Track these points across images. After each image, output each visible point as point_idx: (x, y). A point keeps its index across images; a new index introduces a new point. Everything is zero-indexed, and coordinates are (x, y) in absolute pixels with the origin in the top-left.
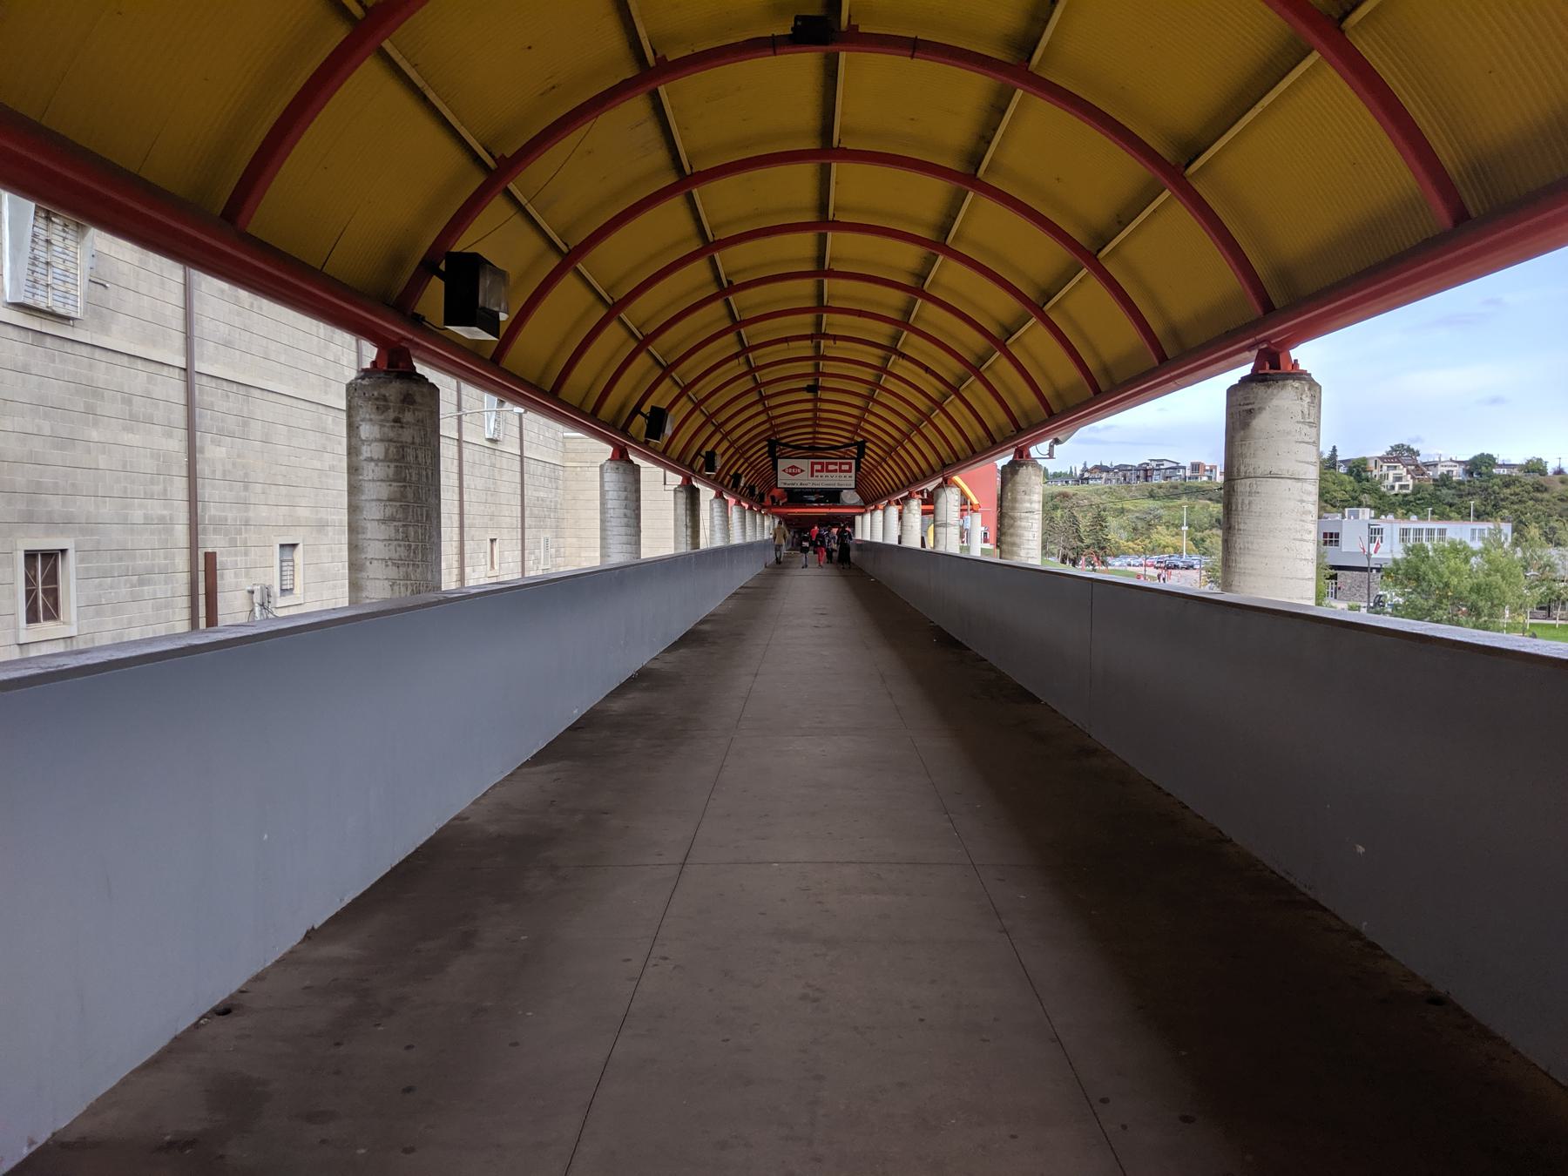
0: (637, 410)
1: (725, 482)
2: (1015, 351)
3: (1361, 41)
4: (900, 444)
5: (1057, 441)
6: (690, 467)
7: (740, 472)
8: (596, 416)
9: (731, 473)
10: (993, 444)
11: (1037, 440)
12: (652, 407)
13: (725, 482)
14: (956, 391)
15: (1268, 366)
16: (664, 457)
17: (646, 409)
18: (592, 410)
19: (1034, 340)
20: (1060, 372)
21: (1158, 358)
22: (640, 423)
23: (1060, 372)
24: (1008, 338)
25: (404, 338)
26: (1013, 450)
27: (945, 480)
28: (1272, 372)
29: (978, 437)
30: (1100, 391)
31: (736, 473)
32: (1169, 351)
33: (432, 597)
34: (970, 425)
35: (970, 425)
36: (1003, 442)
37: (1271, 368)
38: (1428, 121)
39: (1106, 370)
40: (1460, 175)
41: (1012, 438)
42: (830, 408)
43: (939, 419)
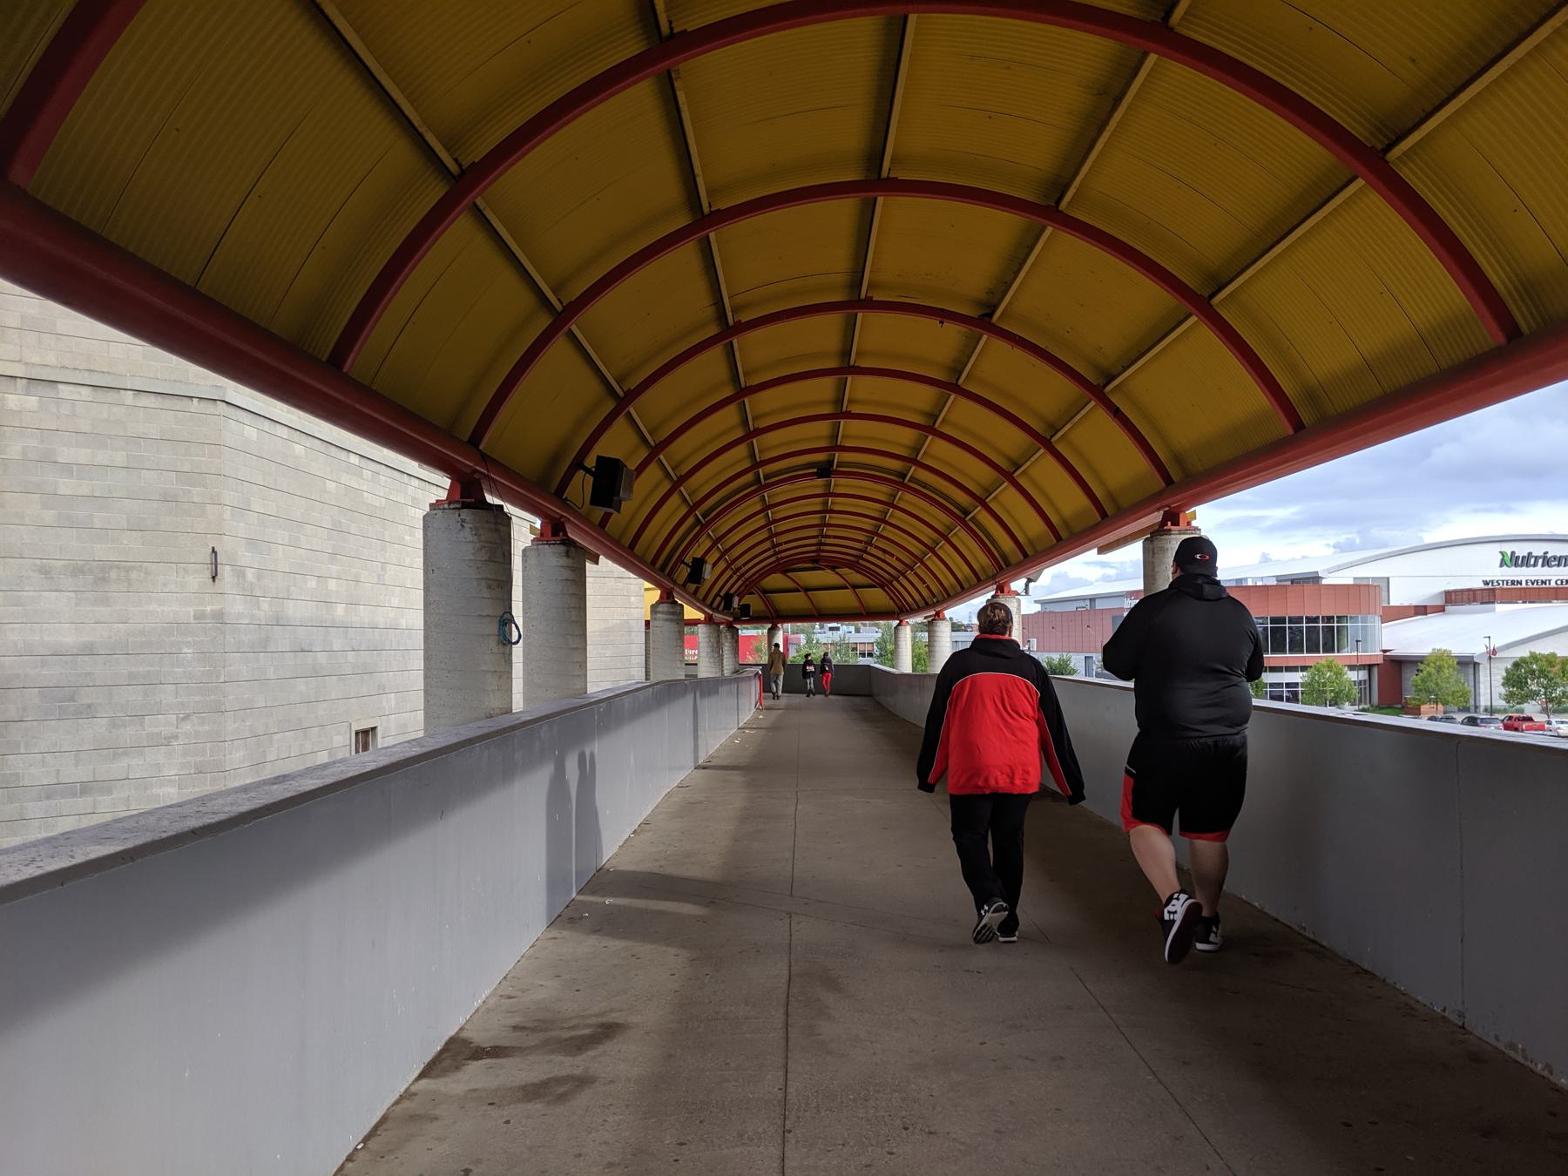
0: (578, 464)
1: (715, 605)
2: (993, 506)
3: (1405, 169)
4: (897, 579)
5: (1030, 580)
6: (710, 606)
7: (732, 592)
8: (339, 366)
9: (722, 594)
10: (927, 606)
11: (1015, 577)
12: (598, 457)
13: (715, 605)
14: (932, 550)
15: (1169, 523)
16: (631, 555)
17: (590, 462)
18: (470, 438)
19: (1044, 473)
20: (1031, 526)
21: (1100, 515)
22: (581, 486)
23: (1068, 501)
24: (988, 497)
25: (563, 516)
26: (995, 586)
27: (938, 614)
28: (1173, 528)
29: (966, 577)
30: (1061, 539)
31: (727, 593)
32: (1109, 510)
33: (505, 721)
34: (943, 573)
35: (943, 573)
36: (986, 580)
37: (1172, 525)
38: (1468, 235)
39: (1112, 497)
40: (1506, 287)
41: (994, 577)
42: (849, 545)
43: (946, 551)
